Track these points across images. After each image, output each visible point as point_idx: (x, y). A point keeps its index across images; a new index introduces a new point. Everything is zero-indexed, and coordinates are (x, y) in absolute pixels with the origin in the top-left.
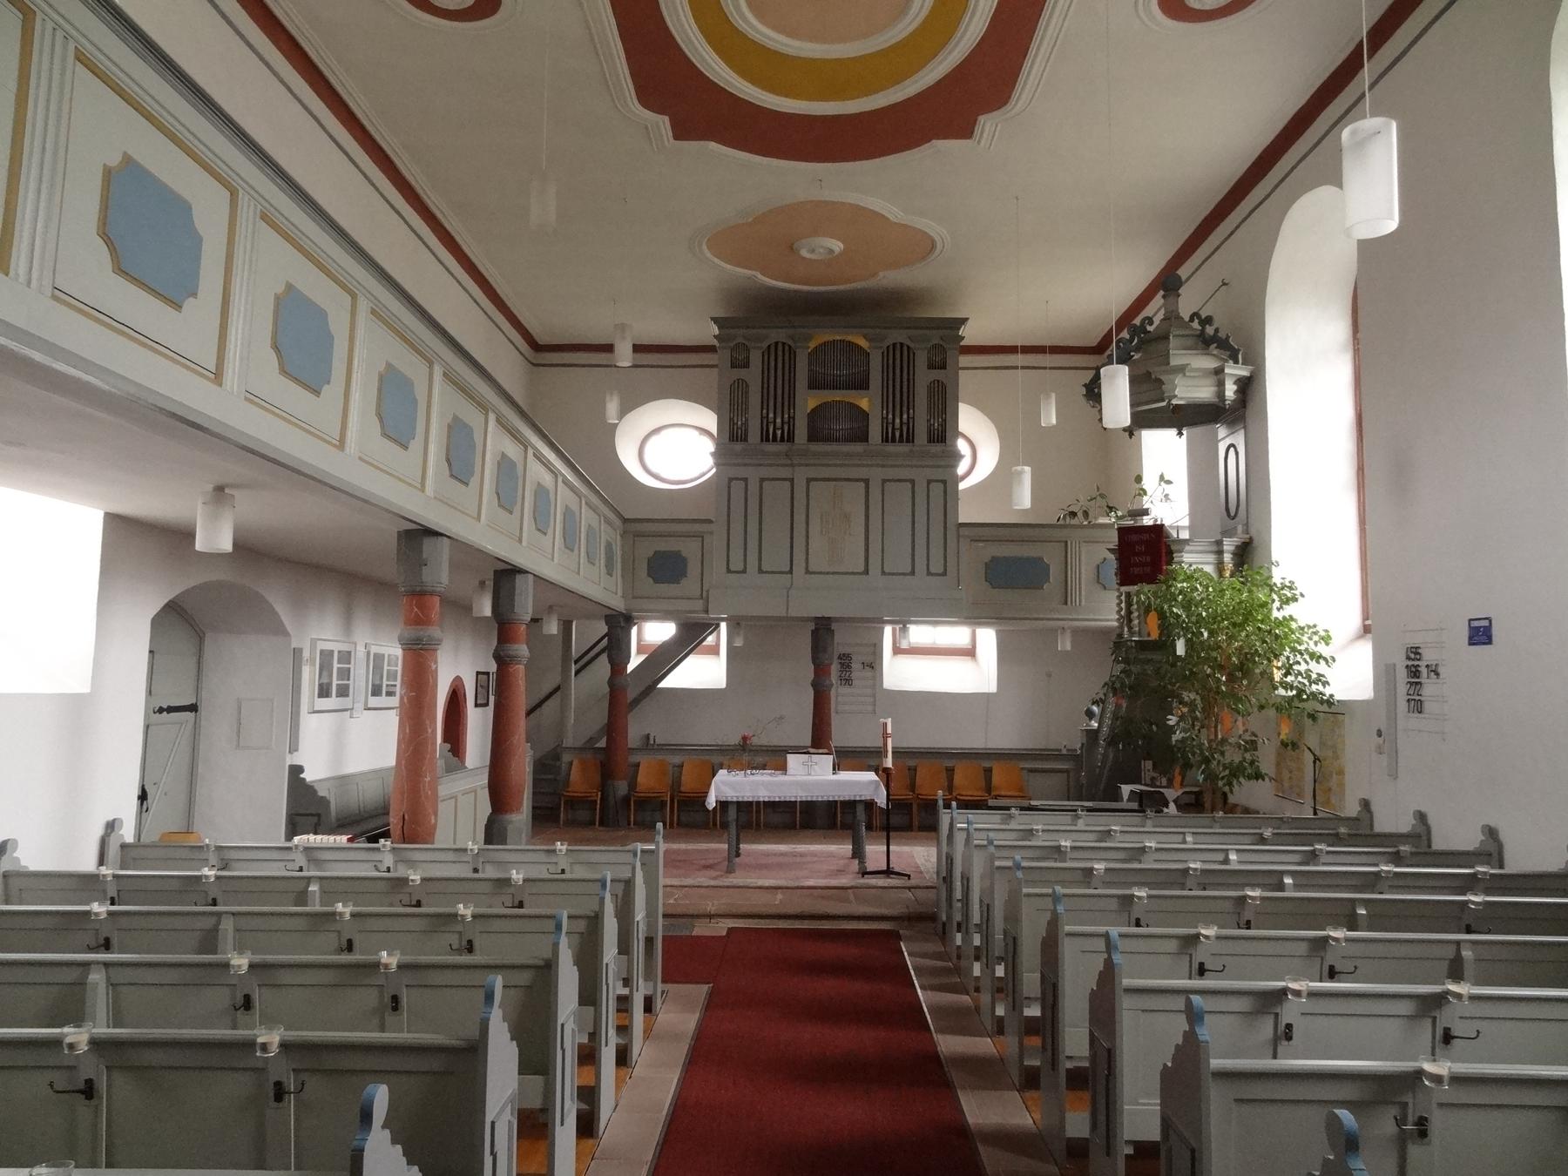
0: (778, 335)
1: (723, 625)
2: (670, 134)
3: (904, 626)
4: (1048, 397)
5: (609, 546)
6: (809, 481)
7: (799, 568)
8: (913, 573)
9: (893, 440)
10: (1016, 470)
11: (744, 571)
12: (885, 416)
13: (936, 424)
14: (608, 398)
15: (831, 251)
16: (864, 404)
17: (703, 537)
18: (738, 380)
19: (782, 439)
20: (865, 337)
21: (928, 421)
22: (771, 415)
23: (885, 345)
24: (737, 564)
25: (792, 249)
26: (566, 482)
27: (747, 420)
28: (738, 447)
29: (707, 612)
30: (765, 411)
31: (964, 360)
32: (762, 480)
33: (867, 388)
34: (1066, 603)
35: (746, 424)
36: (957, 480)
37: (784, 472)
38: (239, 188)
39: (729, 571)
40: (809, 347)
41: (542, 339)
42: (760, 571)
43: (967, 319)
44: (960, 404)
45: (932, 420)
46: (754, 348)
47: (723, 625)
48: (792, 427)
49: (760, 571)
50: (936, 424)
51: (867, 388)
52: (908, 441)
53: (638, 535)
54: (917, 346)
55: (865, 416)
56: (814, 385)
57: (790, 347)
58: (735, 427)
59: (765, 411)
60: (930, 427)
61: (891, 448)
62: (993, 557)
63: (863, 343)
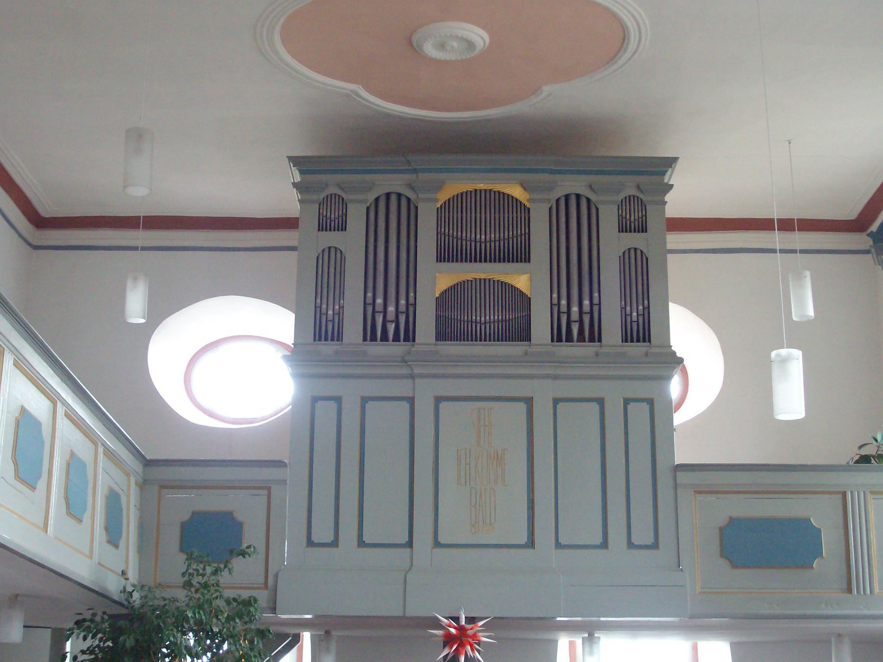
0: (395, 183)
1: (306, 637)
2: (375, 342)
3: (591, 635)
4: (799, 277)
5: (113, 501)
6: (439, 400)
7: (423, 537)
8: (605, 545)
9: (569, 339)
10: (778, 355)
11: (335, 543)
12: (555, 301)
13: (635, 314)
14: (130, 284)
15: (471, 45)
16: (522, 282)
17: (269, 489)
18: (330, 248)
19: (396, 338)
20: (522, 185)
21: (624, 308)
22: (379, 301)
23: (554, 196)
24: (323, 533)
25: (411, 43)
26: (72, 417)
27: (341, 307)
28: (328, 348)
29: (274, 610)
30: (370, 294)
31: (674, 240)
32: (365, 400)
33: (528, 260)
34: (850, 590)
35: (340, 314)
36: (670, 409)
37: (402, 388)
38: (58, 401)
39: (310, 543)
40: (437, 200)
41: (47, 208)
42: (361, 543)
43: (675, 159)
44: (670, 303)
45: (628, 308)
46: (353, 201)
47: (306, 637)
48: (411, 319)
49: (361, 543)
50: (635, 314)
51: (528, 260)
52: (592, 340)
53: (165, 486)
54: (601, 198)
55: (524, 301)
56: (445, 255)
57: (409, 200)
58: (324, 318)
59: (370, 294)
60: (625, 316)
61: (565, 350)
62: (731, 519)
63: (517, 192)
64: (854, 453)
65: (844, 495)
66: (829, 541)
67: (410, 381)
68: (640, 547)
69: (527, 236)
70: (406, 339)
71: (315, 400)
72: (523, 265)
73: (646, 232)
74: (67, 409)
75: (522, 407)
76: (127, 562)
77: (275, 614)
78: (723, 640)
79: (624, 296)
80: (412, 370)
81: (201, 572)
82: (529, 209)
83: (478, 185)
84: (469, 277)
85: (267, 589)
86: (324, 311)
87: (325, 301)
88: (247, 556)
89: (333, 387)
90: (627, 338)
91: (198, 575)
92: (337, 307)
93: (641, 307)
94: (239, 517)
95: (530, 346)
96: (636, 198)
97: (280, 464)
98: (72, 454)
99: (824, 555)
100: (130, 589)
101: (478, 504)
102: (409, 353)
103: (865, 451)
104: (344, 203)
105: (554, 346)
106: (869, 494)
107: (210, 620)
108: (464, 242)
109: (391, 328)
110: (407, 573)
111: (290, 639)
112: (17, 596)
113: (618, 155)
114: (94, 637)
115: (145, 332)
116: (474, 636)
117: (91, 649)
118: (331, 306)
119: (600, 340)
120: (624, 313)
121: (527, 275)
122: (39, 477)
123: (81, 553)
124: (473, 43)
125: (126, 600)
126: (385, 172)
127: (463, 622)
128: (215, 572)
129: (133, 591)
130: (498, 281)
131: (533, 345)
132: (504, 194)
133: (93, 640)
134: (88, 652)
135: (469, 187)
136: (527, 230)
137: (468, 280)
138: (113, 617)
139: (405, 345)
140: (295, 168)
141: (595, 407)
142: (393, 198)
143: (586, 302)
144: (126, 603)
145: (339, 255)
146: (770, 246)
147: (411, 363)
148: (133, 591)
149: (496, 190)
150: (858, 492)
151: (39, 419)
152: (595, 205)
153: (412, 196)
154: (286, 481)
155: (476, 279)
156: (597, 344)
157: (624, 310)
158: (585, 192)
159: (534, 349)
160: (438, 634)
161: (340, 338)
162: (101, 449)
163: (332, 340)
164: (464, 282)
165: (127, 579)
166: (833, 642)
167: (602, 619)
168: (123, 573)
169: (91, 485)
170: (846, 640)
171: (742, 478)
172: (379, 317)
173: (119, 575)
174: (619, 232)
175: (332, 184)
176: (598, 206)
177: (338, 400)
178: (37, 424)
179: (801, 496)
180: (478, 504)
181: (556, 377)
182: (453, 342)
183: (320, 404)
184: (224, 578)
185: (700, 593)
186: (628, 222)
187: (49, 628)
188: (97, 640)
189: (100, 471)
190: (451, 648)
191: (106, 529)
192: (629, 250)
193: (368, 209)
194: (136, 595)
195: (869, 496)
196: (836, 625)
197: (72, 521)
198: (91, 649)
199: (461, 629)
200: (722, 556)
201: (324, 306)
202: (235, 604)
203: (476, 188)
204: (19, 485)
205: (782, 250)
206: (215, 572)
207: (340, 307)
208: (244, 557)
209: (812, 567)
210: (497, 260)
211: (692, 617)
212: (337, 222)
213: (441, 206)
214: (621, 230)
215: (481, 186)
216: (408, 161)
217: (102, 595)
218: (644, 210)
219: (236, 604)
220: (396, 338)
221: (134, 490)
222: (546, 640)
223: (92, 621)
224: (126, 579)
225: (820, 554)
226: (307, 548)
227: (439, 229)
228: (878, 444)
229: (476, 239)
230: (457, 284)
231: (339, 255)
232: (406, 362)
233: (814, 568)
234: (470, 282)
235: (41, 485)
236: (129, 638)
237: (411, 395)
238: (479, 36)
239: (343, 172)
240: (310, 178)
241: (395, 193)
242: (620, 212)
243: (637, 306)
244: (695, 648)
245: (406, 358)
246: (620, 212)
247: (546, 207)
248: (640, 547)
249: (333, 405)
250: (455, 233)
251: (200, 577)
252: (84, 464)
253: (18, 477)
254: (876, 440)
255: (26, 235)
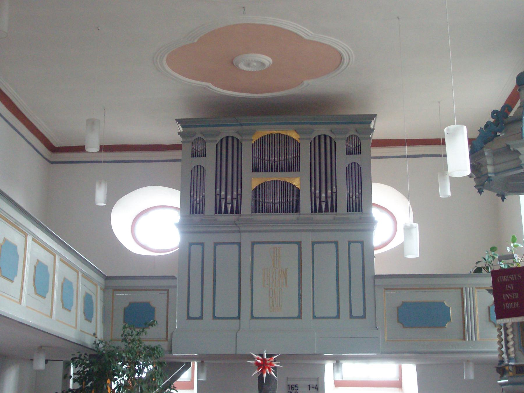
5: (88, 300)
6: (253, 244)
8: (338, 317)
9: (320, 210)
11: (201, 318)
12: (313, 191)
13: (354, 197)
14: (97, 186)
15: (263, 64)
16: (296, 182)
17: (168, 290)
19: (232, 212)
21: (348, 194)
23: (312, 137)
24: (195, 312)
25: (232, 63)
28: (197, 218)
29: (171, 352)
32: (216, 244)
33: (299, 170)
34: (464, 339)
35: (203, 200)
39: (189, 318)
40: (252, 140)
41: (57, 143)
47: (195, 364)
50: (354, 197)
51: (299, 170)
53: (116, 290)
55: (297, 192)
56: (257, 168)
57: (238, 140)
58: (195, 202)
59: (218, 190)
60: (349, 198)
61: (319, 216)
63: (294, 135)
64: (472, 268)
65: (462, 289)
66: (454, 314)
67: (239, 234)
68: (356, 317)
69: (298, 157)
70: (237, 213)
71: (191, 244)
72: (297, 173)
73: (360, 154)
74: (61, 258)
75: (296, 247)
76: (96, 328)
77: (171, 353)
78: (412, 363)
79: (348, 187)
80: (240, 229)
81: (130, 334)
82: (299, 143)
83: (273, 131)
84: (268, 179)
85: (167, 341)
86: (195, 199)
87: (195, 194)
88: (154, 326)
89: (199, 238)
90: (350, 210)
91: (129, 336)
92: (201, 197)
93: (357, 194)
94: (153, 304)
95: (300, 215)
96: (355, 136)
97: (173, 278)
98: (65, 278)
99: (451, 320)
100: (98, 342)
101: (273, 297)
102: (238, 220)
103: (479, 265)
104: (205, 142)
105: (312, 214)
106: (475, 288)
107: (136, 357)
108: (266, 161)
109: (229, 207)
110: (237, 332)
111: (184, 365)
112: (41, 347)
113: (344, 114)
114: (80, 366)
115: (108, 210)
116: (270, 364)
117: (79, 372)
118: (198, 196)
119: (336, 211)
120: (348, 196)
121: (298, 178)
122: (47, 292)
123: (71, 326)
124: (264, 63)
125: (96, 348)
126: (225, 125)
127: (265, 357)
128: (138, 334)
129: (99, 343)
130: (284, 181)
131: (302, 214)
132: (287, 136)
133: (80, 368)
134: (77, 374)
135: (269, 133)
136: (298, 154)
137: (268, 181)
138: (90, 356)
139: (236, 216)
140: (179, 125)
141: (333, 246)
142: (230, 140)
143: (329, 191)
144: (96, 349)
145: (202, 169)
146: (438, 153)
147: (239, 225)
148: (99, 343)
149: (282, 134)
150: (469, 288)
151: (46, 264)
152: (334, 141)
153: (239, 137)
154: (176, 286)
155: (272, 181)
156: (335, 213)
157: (349, 195)
158: (329, 134)
159: (301, 216)
160: (252, 363)
161: (203, 213)
162: (80, 274)
163: (199, 213)
164: (266, 182)
165: (96, 337)
166: (464, 364)
167: (343, 354)
168: (94, 334)
169: (75, 293)
170: (471, 363)
171: (412, 281)
172: (223, 200)
173: (92, 335)
174: (346, 154)
175: (198, 132)
176: (335, 141)
177: (202, 244)
178: (45, 267)
179: (436, 290)
180: (273, 297)
181: (313, 231)
182: (259, 214)
183: (193, 247)
184: (143, 336)
185: (388, 341)
186: (351, 149)
187: (62, 361)
188: (82, 368)
189: (80, 284)
190: (259, 370)
191: (84, 313)
192: (352, 163)
193: (217, 145)
194: (101, 345)
195: (475, 290)
196: (464, 356)
197: (66, 312)
198: (79, 372)
199: (264, 360)
200: (398, 322)
201: (195, 196)
202: (148, 349)
203: (272, 133)
204: (37, 296)
205: (441, 157)
206: (138, 334)
207: (203, 196)
208: (152, 326)
209: (444, 327)
210: (286, 171)
211: (382, 353)
212: (201, 152)
213: (254, 143)
214: (347, 153)
215: (275, 132)
216: (237, 120)
217: (83, 346)
218: (359, 142)
219: (148, 349)
220: (232, 212)
221: (100, 293)
222: (318, 364)
223: (79, 358)
224: (96, 337)
225: (448, 320)
226: (187, 320)
227: (253, 155)
228: (486, 261)
229: (272, 160)
230: (263, 184)
231: (202, 169)
232: (236, 224)
233: (446, 328)
234: (269, 182)
235: (49, 295)
236: (95, 367)
237: (239, 241)
238: (267, 60)
239: (204, 126)
240: (189, 129)
241: (230, 136)
242: (347, 144)
243: (356, 194)
244: (400, 368)
245: (236, 223)
246: (347, 144)
247: (309, 142)
248: (356, 317)
249: (200, 247)
250: (261, 157)
251: (130, 337)
252: (71, 283)
253: (36, 293)
254: (485, 259)
255: (48, 157)
